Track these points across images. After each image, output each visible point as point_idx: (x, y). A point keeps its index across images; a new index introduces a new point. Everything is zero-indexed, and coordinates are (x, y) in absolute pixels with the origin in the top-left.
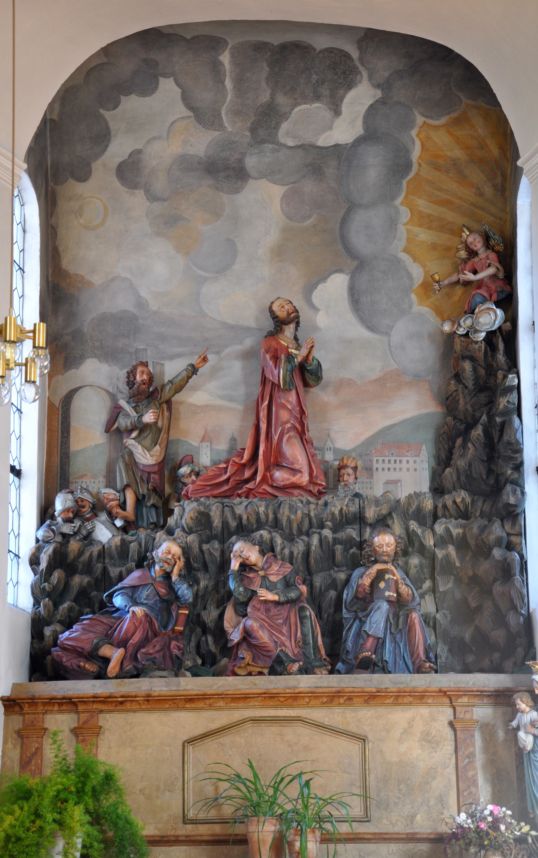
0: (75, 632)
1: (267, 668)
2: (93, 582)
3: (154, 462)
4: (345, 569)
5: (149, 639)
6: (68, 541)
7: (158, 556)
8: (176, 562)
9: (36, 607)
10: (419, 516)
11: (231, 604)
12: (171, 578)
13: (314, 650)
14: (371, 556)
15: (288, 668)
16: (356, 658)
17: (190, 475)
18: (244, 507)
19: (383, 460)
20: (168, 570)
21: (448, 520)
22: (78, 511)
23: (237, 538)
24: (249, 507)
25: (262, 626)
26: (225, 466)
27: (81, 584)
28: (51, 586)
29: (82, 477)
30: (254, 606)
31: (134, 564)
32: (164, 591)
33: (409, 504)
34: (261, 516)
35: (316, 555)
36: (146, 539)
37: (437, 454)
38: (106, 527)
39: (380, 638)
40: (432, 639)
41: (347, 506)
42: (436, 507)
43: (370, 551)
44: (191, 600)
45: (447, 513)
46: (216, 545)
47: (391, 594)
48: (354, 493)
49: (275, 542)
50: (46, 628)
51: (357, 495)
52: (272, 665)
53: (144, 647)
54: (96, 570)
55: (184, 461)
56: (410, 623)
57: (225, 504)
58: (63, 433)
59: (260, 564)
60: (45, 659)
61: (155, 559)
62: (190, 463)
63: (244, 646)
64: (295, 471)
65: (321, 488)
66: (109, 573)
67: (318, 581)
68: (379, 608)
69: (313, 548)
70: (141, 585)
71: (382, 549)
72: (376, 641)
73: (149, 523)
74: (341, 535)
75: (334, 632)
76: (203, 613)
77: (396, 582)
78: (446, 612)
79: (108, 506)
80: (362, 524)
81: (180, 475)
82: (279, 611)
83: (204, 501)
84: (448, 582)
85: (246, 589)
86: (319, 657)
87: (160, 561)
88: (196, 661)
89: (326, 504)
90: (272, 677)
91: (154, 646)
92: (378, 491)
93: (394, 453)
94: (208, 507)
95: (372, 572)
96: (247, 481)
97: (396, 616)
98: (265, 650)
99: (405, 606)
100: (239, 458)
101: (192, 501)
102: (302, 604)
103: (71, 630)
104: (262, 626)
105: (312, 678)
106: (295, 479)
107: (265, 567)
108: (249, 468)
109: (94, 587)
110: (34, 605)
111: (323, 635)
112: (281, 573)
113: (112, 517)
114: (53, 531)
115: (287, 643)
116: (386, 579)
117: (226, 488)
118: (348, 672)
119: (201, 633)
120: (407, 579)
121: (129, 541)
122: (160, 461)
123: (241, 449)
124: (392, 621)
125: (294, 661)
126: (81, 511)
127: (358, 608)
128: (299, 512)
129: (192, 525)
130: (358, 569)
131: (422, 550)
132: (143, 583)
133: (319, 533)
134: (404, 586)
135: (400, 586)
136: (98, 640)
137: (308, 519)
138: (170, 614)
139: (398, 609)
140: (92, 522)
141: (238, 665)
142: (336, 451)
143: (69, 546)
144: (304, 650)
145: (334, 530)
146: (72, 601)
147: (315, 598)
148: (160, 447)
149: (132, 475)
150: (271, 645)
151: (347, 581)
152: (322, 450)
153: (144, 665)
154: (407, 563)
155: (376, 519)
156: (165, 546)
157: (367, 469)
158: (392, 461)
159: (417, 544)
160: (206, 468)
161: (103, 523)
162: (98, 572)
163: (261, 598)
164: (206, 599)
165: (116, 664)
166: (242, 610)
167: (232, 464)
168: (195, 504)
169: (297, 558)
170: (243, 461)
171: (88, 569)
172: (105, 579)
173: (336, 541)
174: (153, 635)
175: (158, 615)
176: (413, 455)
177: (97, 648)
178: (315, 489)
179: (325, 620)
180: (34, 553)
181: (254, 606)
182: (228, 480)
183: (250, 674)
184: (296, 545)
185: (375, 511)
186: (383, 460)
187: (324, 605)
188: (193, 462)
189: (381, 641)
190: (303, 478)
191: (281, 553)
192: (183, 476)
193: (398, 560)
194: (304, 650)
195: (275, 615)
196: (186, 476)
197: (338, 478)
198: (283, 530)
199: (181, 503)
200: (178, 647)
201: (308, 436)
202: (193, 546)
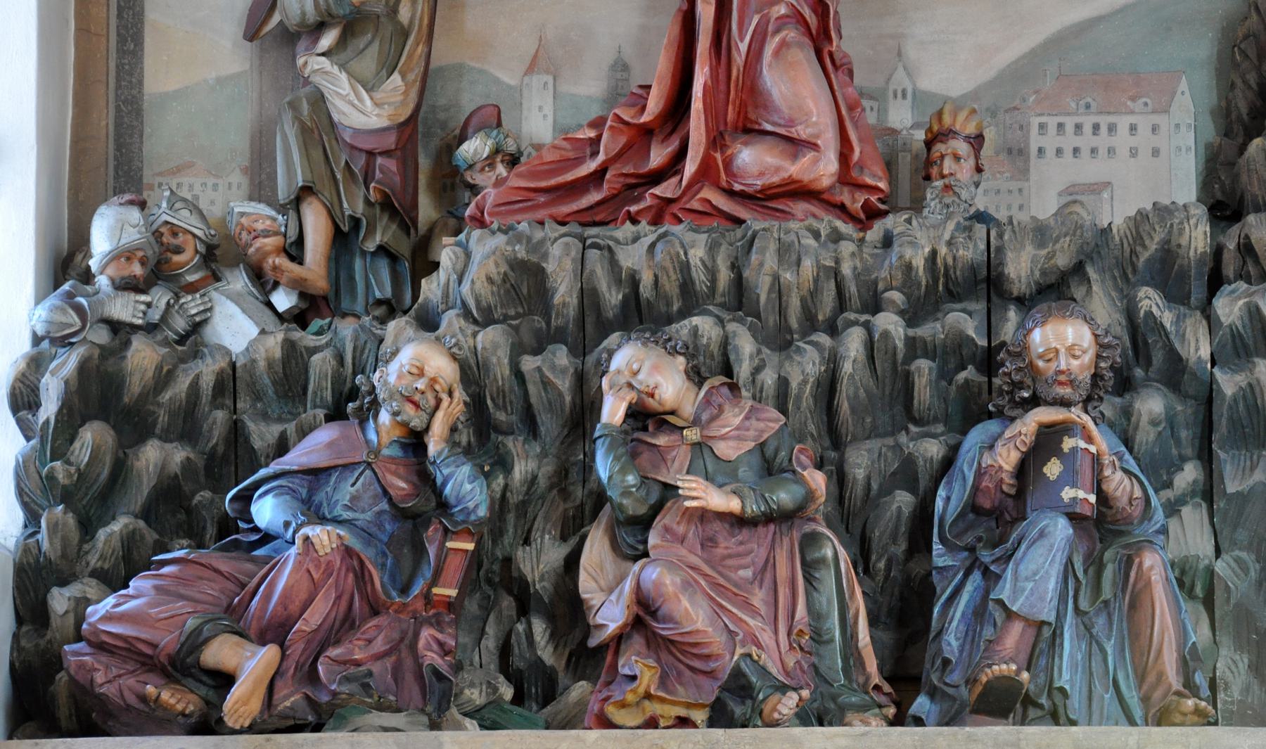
0: (133, 597)
1: (703, 706)
2: (200, 463)
3: (384, 123)
4: (940, 428)
5: (354, 622)
6: (127, 344)
7: (386, 383)
8: (439, 401)
9: (30, 531)
10: (1167, 273)
11: (603, 526)
12: (425, 447)
13: (845, 660)
14: (1019, 386)
15: (767, 708)
16: (971, 681)
17: (490, 162)
18: (646, 248)
19: (1061, 126)
20: (417, 422)
21: (1254, 288)
22: (159, 263)
23: (622, 337)
24: (659, 247)
25: (687, 585)
26: (592, 134)
27: (163, 467)
28: (73, 469)
29: (178, 170)
30: (667, 529)
31: (321, 413)
32: (403, 485)
33: (1138, 239)
34: (694, 274)
35: (857, 388)
36: (356, 339)
37: (1223, 104)
38: (244, 311)
39: (1043, 623)
40: (1200, 634)
41: (950, 243)
42: (1218, 252)
43: (1019, 370)
44: (482, 512)
45: (1251, 268)
46: (561, 356)
47: (1080, 495)
48: (972, 210)
49: (736, 348)
50: (55, 591)
51: (981, 217)
52: (718, 699)
53: (337, 642)
54: (211, 430)
55: (474, 121)
56: (1134, 586)
57: (589, 242)
58: (122, 40)
59: (688, 410)
60: (51, 679)
61: (378, 391)
62: (490, 127)
63: (637, 641)
64: (796, 145)
65: (873, 199)
66: (247, 440)
67: (861, 462)
68: (1042, 534)
69: (847, 367)
70: (335, 467)
71: (1053, 365)
72: (1031, 632)
73: (371, 301)
74: (929, 330)
75: (907, 614)
76: (520, 553)
77: (1096, 460)
78: (1244, 555)
79: (251, 250)
80: (994, 298)
81: (460, 163)
82: (741, 543)
83: (528, 231)
84: (1252, 469)
85: (644, 479)
86: (861, 680)
87: (391, 397)
88: (496, 690)
89: (887, 241)
90: (718, 732)
91: (370, 641)
92: (1045, 206)
93: (1093, 104)
94: (538, 247)
95: (1024, 430)
96: (657, 177)
97: (1095, 564)
98: (695, 655)
99: (1121, 533)
100: (633, 111)
101: (493, 233)
102: (809, 528)
103: (123, 592)
104: (687, 585)
105: (836, 735)
106: (798, 168)
107: (705, 417)
108: (663, 141)
109: (202, 479)
110: (26, 526)
111: (873, 622)
112: (752, 433)
113: (263, 281)
114: (79, 310)
115: (766, 638)
116: (1066, 450)
117: (594, 197)
118: (950, 720)
119: (514, 613)
120: (1127, 456)
121: (307, 349)
122: (402, 119)
123: (641, 87)
124: (1080, 574)
125: (783, 689)
126: (168, 261)
127: (980, 539)
128: (808, 264)
129: (491, 300)
130: (980, 426)
131: (1175, 374)
132: (340, 462)
133: (867, 326)
134: (1119, 474)
135: (1107, 472)
136: (200, 621)
137: (832, 284)
138: (419, 551)
139: (1099, 546)
140: (202, 296)
141: (617, 697)
142: (919, 98)
143: (129, 354)
144: (814, 659)
145: (912, 316)
146: (136, 517)
147: (851, 515)
148: (403, 77)
149: (322, 158)
150: (715, 639)
151: (948, 463)
152: (878, 96)
153: (334, 694)
154: (1127, 412)
155: (1037, 283)
156: (406, 356)
157: (1010, 151)
158: (1088, 129)
159: (1158, 357)
160: (538, 147)
161: (236, 299)
162: (216, 433)
163: (688, 504)
164: (530, 515)
165: (251, 694)
166: (632, 535)
167: (611, 127)
168: (501, 239)
169: (799, 397)
170: (645, 118)
171: (186, 426)
172: (236, 458)
173: (915, 348)
174: (367, 609)
175: (384, 554)
176: (1150, 108)
177: (196, 642)
178: (856, 202)
179: (880, 578)
180: (23, 375)
181: (667, 529)
182: (599, 175)
183: (652, 723)
184: (798, 358)
185: (1034, 260)
186: (1061, 126)
187: (878, 534)
188: (499, 124)
189: (1047, 632)
190: (822, 165)
191: (754, 381)
192: (471, 167)
193: (1101, 399)
194: (814, 659)
195: (730, 556)
196: (478, 166)
197: (926, 169)
198: (758, 316)
199: (462, 236)
200: (441, 644)
201: (838, 46)
202: (494, 360)
